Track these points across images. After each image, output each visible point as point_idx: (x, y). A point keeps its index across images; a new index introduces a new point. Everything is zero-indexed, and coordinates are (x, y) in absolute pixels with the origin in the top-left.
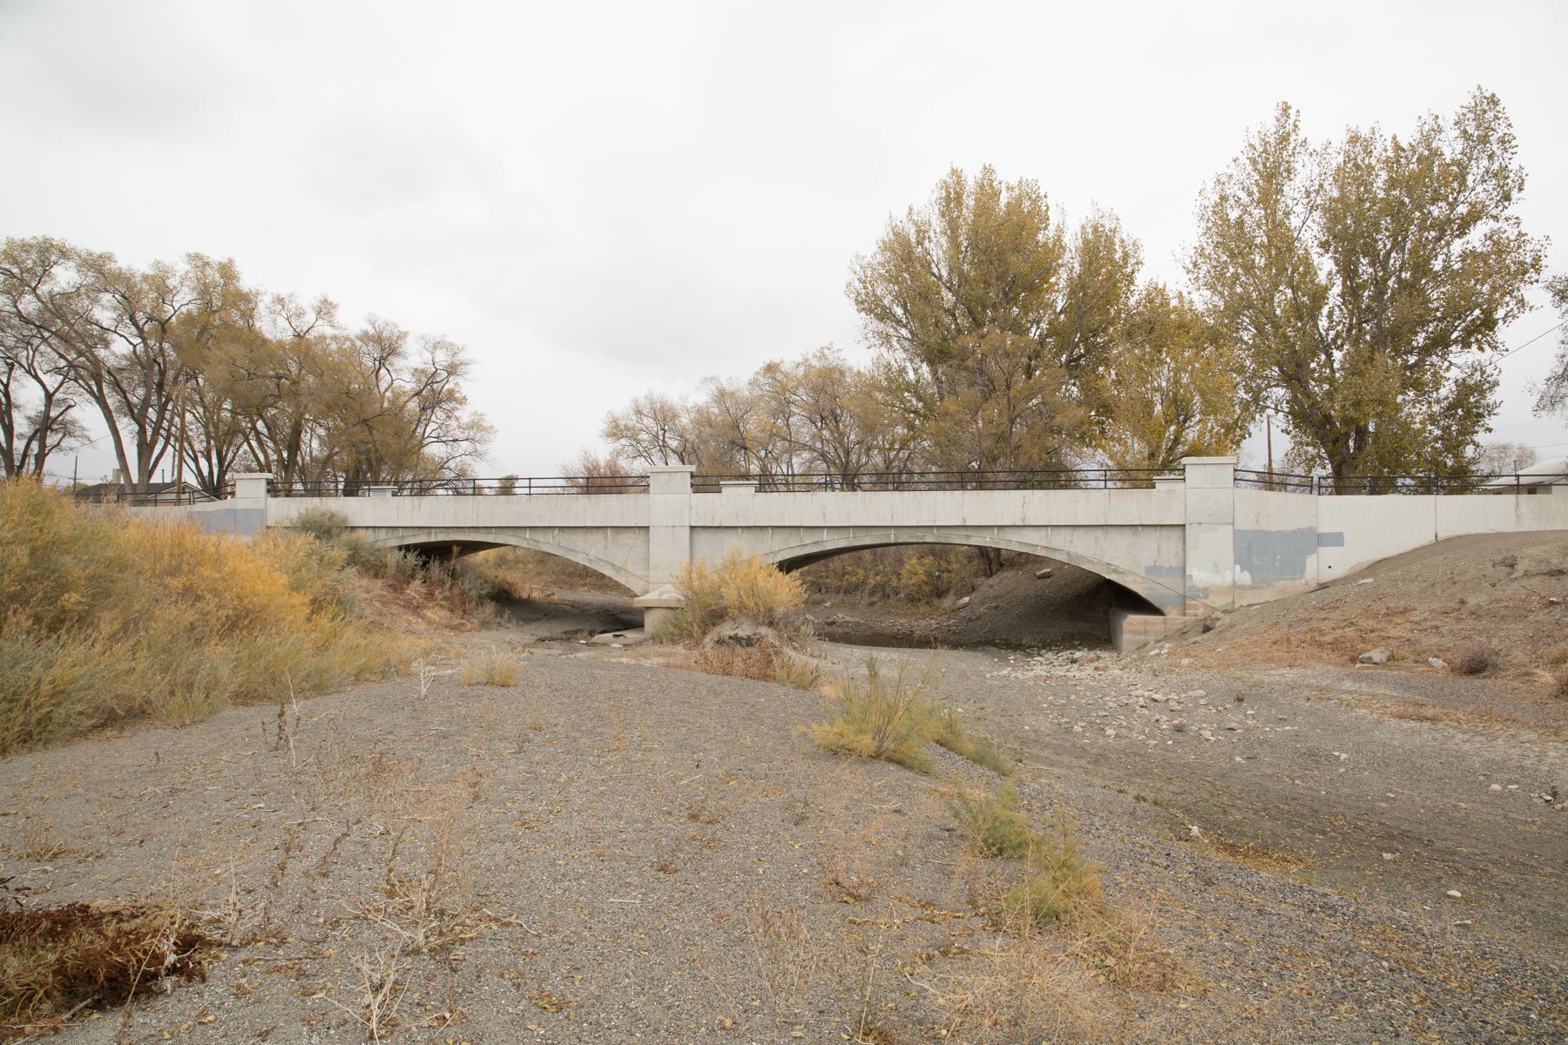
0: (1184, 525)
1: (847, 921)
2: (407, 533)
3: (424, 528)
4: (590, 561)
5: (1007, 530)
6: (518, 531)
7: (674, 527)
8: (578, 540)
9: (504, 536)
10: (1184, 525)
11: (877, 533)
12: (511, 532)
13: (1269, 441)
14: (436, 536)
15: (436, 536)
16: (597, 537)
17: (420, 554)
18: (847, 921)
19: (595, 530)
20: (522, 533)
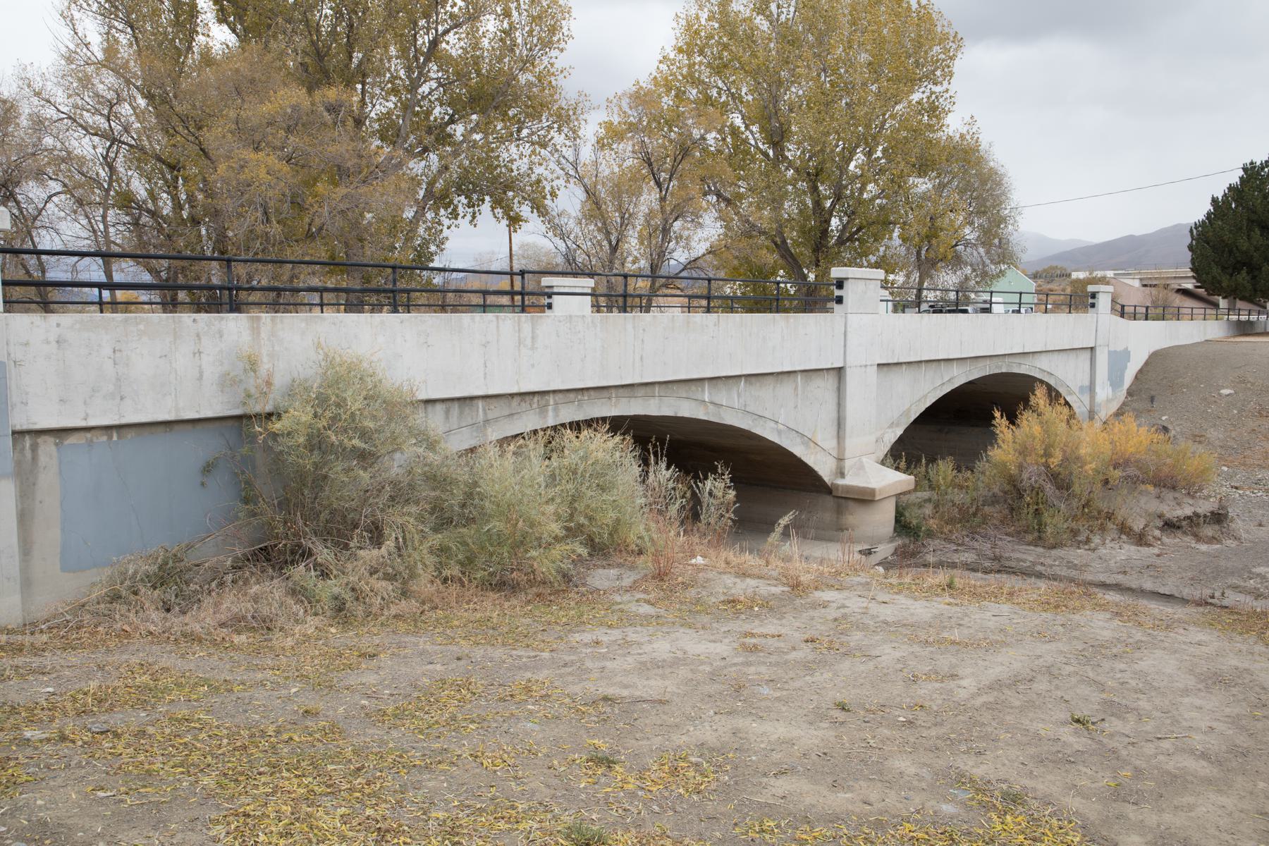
0: (840, 371)
1: (786, 41)
2: (497, 410)
3: (533, 393)
4: (779, 432)
5: (1036, 356)
6: (670, 386)
7: (866, 366)
8: (723, 396)
9: (672, 400)
10: (840, 371)
11: (981, 364)
12: (683, 391)
13: (845, 346)
14: (556, 410)
15: (556, 410)
16: (786, 390)
17: (450, 136)
18: (786, 41)
19: (785, 377)
20: (694, 391)
